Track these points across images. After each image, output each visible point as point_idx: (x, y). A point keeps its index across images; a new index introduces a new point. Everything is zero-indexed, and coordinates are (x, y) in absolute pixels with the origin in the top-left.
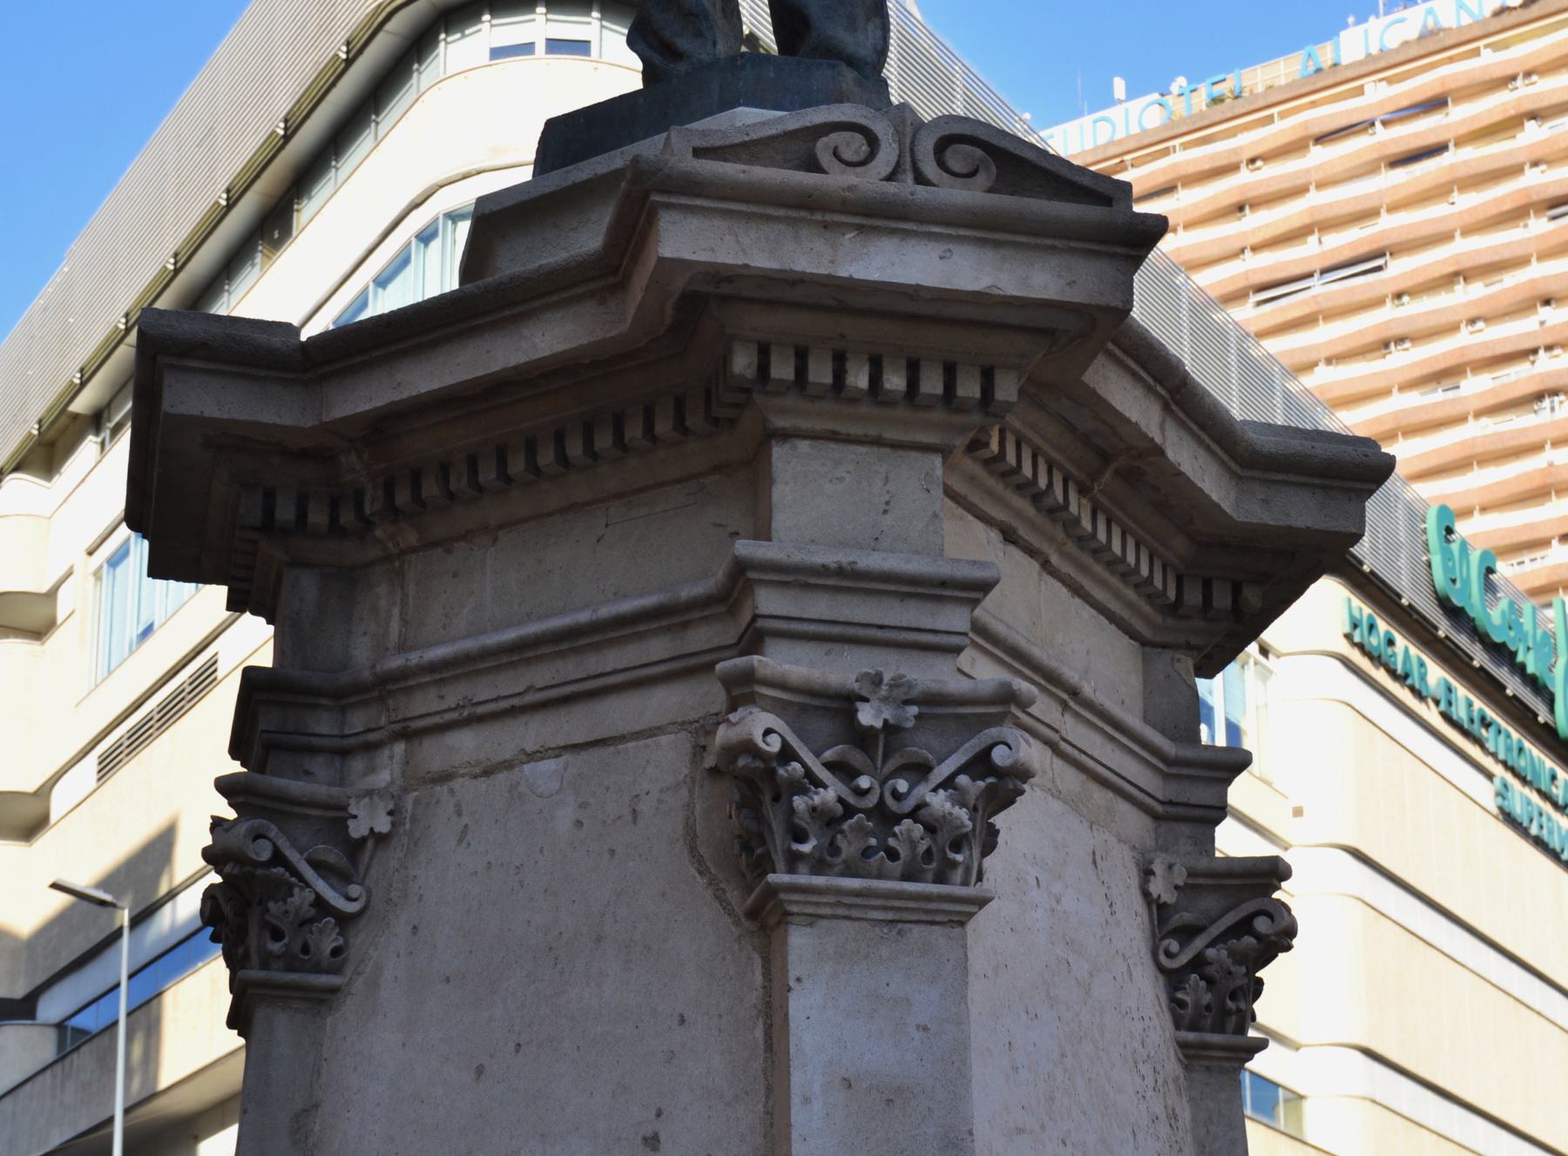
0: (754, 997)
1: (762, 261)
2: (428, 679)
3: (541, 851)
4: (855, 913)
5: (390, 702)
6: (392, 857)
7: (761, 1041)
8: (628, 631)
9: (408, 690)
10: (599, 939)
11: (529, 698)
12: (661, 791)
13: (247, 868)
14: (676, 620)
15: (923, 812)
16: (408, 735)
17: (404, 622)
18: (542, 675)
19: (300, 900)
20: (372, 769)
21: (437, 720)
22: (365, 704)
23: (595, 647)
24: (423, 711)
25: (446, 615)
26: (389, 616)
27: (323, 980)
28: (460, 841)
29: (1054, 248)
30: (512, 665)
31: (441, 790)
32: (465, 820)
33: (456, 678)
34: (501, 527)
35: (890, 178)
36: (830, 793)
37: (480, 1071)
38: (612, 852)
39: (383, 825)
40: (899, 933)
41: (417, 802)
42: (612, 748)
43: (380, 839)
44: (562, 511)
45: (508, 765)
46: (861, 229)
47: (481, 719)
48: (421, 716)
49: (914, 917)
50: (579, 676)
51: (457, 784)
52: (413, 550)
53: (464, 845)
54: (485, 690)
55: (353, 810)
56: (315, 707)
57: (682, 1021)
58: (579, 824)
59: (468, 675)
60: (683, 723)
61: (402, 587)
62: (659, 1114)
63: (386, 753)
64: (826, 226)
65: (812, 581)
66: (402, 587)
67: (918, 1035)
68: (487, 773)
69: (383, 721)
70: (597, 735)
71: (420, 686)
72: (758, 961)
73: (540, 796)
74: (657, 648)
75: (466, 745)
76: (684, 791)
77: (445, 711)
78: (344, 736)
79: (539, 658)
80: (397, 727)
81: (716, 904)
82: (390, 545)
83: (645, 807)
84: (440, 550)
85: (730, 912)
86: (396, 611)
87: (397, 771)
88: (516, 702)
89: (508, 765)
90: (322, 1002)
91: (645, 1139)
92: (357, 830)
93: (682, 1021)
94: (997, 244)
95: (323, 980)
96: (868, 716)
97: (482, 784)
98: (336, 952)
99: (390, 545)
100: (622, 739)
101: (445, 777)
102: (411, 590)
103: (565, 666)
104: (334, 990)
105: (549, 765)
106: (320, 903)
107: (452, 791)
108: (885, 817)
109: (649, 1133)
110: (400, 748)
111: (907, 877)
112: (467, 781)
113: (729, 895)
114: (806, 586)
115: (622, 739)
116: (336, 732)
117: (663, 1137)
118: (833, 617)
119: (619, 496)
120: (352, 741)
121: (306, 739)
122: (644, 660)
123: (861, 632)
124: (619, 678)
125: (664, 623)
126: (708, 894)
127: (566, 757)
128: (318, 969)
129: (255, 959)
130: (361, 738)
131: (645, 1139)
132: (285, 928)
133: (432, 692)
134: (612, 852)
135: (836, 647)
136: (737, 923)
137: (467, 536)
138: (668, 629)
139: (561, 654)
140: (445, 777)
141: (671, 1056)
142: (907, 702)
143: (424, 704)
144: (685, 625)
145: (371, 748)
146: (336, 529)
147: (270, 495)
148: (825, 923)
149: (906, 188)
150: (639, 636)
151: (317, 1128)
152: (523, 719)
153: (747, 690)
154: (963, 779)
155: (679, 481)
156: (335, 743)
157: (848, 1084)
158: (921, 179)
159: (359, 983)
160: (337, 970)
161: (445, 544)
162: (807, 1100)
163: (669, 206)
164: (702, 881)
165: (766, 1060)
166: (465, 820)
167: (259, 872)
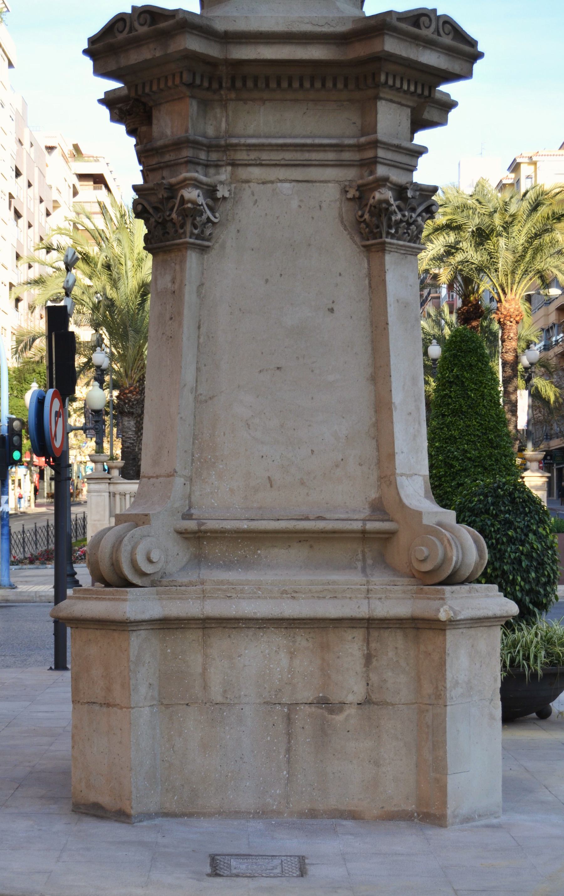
0: (365, 271)
1: (404, 54)
2: (245, 148)
3: (286, 213)
4: (399, 251)
5: (227, 152)
6: (228, 205)
7: (367, 284)
8: (322, 149)
9: (235, 150)
10: (309, 245)
11: (282, 162)
12: (330, 201)
13: (195, 206)
14: (340, 149)
15: (416, 223)
16: (234, 164)
17: (227, 123)
18: (288, 156)
19: (204, 217)
20: (218, 173)
21: (246, 162)
22: (218, 151)
23: (309, 151)
24: (241, 158)
25: (245, 126)
26: (221, 121)
27: (206, 243)
28: (254, 204)
29: (460, 58)
30: (277, 150)
31: (246, 186)
32: (256, 197)
33: (255, 150)
34: (267, 100)
35: (433, 33)
36: (399, 216)
37: (267, 281)
38: (313, 218)
39: (227, 195)
40: (406, 257)
41: (235, 188)
42: (311, 184)
43: (224, 198)
44: (291, 100)
45: (272, 182)
46: (424, 47)
47: (261, 165)
48: (239, 160)
49: (409, 253)
50: (302, 159)
51: (251, 184)
52: (231, 100)
53: (256, 206)
54: (265, 156)
55: (218, 188)
56: (201, 149)
57: (340, 275)
58: (300, 207)
59: (260, 150)
60: (337, 181)
61: (226, 112)
62: (333, 302)
63: (224, 169)
64: (417, 45)
65: (390, 148)
66: (226, 112)
67: (410, 287)
68: (264, 183)
69: (225, 158)
70: (306, 179)
71: (241, 150)
72: (366, 261)
73: (285, 195)
74: (331, 156)
75: (256, 172)
76: (338, 203)
77: (249, 160)
78: (208, 161)
79: (288, 150)
80: (231, 162)
81: (351, 241)
82: (224, 97)
83: (324, 205)
84: (242, 102)
85: (356, 244)
86: (224, 120)
87: (229, 176)
88: (278, 162)
89: (272, 182)
90: (203, 250)
91: (329, 309)
92: (219, 195)
93: (340, 275)
94: (449, 55)
95: (206, 243)
96: (410, 194)
97: (262, 187)
98: (210, 234)
99: (224, 97)
100: (315, 182)
101: (247, 181)
102: (230, 113)
103: (299, 155)
104: (208, 247)
105: (287, 185)
106: (208, 218)
107: (249, 187)
108: (409, 224)
109: (330, 308)
110: (229, 168)
111: (409, 241)
112: (256, 185)
113: (355, 238)
114: (388, 149)
115: (315, 182)
116: (206, 159)
117: (335, 309)
118: (385, 157)
119: (313, 100)
120: (212, 163)
121: (199, 160)
122: (326, 159)
123: (401, 165)
124: (317, 163)
125: (335, 149)
126: (348, 237)
127: (293, 184)
128: (203, 239)
129: (188, 234)
130: (216, 163)
131: (329, 309)
132: (199, 225)
133: (245, 153)
134: (313, 218)
135: (391, 168)
136: (359, 247)
137: (254, 100)
138: (336, 151)
139: (296, 151)
140: (247, 181)
141: (337, 285)
142: (416, 190)
143: (241, 156)
144: (342, 151)
145: (217, 166)
146: (209, 89)
147: (194, 75)
148: (392, 253)
149: (435, 37)
150: (325, 151)
151: (203, 291)
152: (278, 168)
153: (384, 183)
154: (424, 214)
155: (335, 101)
156: (205, 162)
157: (398, 301)
158: (439, 34)
159: (217, 246)
160: (208, 240)
161: (245, 101)
162: (390, 305)
163: (388, 34)
164: (345, 233)
165: (369, 290)
166: (256, 197)
167: (198, 207)
